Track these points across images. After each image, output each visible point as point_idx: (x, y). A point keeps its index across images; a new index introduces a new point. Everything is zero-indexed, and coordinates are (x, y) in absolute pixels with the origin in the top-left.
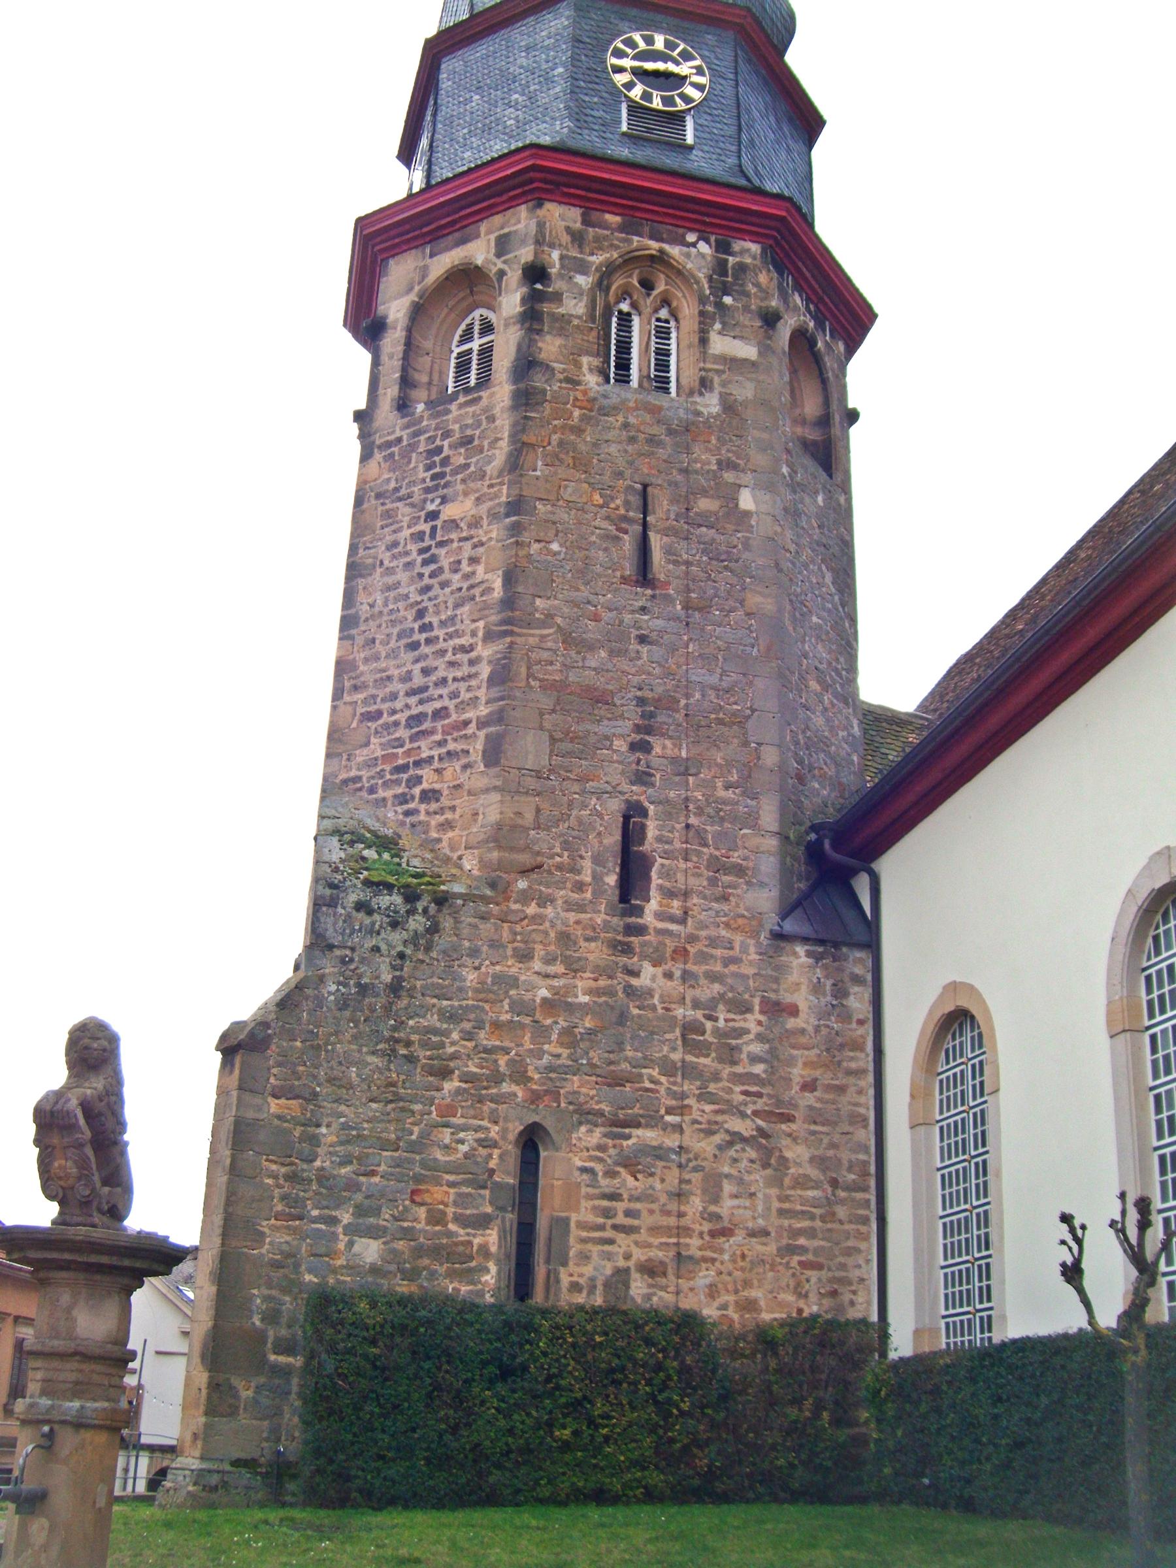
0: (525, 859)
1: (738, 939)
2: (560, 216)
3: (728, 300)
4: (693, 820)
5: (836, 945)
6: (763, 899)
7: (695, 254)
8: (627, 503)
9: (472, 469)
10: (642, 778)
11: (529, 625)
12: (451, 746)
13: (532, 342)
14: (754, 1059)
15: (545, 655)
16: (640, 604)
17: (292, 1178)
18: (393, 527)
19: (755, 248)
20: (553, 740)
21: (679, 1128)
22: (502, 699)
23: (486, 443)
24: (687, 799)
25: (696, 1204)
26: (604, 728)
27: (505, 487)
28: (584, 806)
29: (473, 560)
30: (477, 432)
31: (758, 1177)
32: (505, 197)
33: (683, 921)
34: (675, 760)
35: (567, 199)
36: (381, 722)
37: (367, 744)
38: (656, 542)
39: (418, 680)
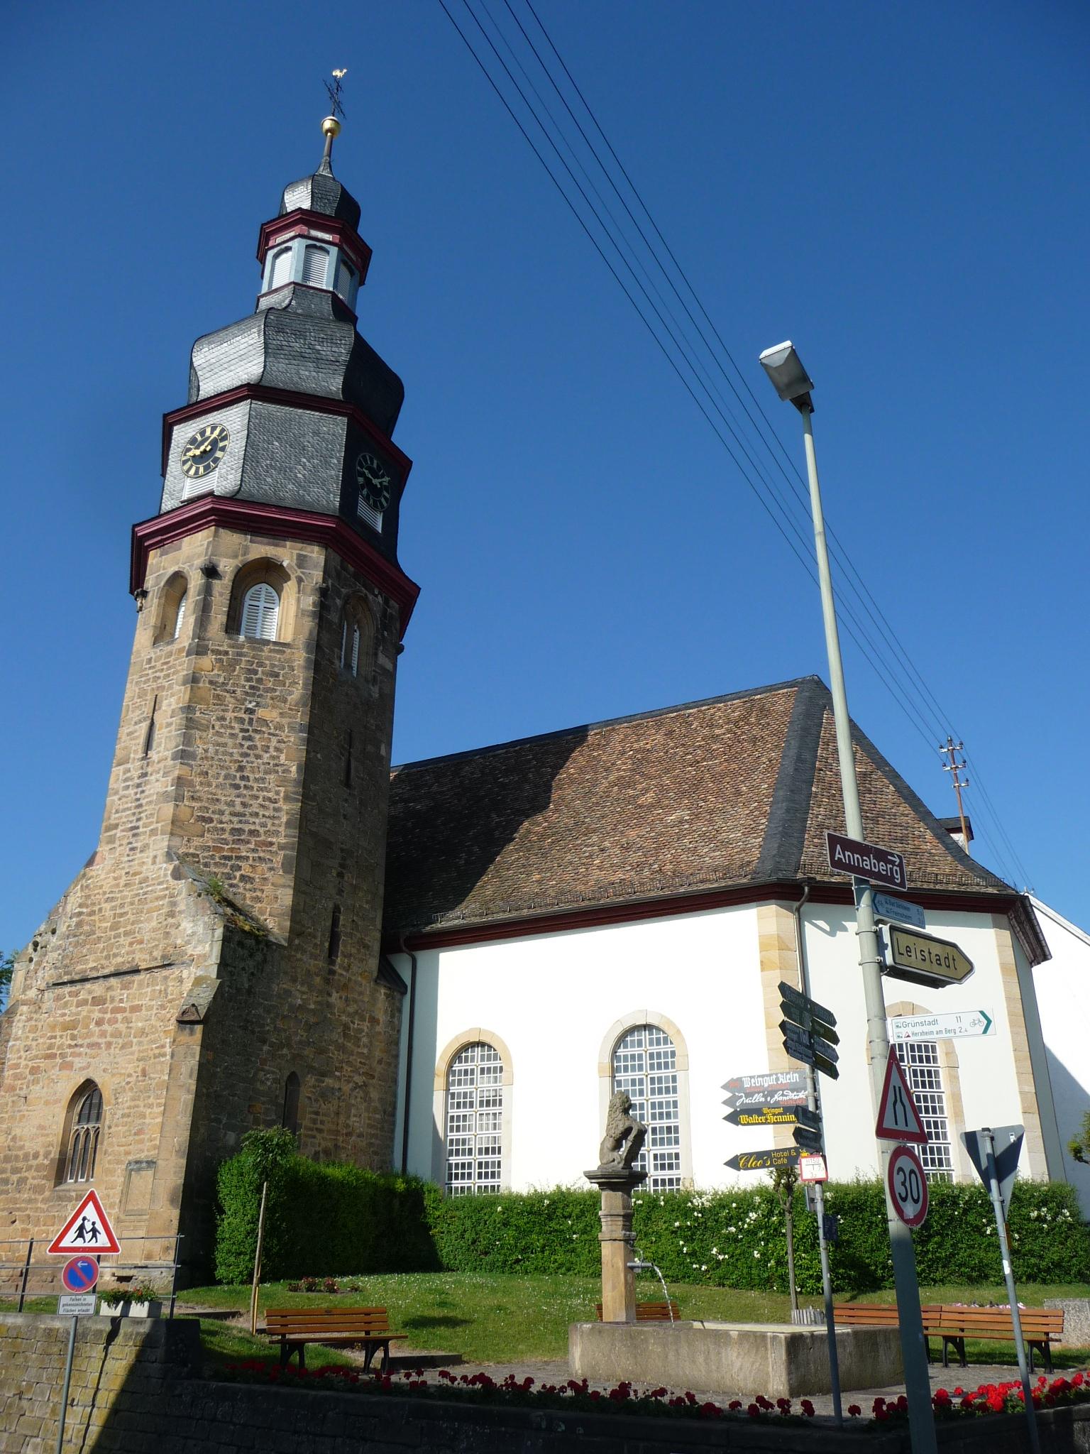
12: (262, 855)
21: (339, 1078)
23: (287, 682)
25: (342, 1119)
33: (347, 971)
37: (202, 836)
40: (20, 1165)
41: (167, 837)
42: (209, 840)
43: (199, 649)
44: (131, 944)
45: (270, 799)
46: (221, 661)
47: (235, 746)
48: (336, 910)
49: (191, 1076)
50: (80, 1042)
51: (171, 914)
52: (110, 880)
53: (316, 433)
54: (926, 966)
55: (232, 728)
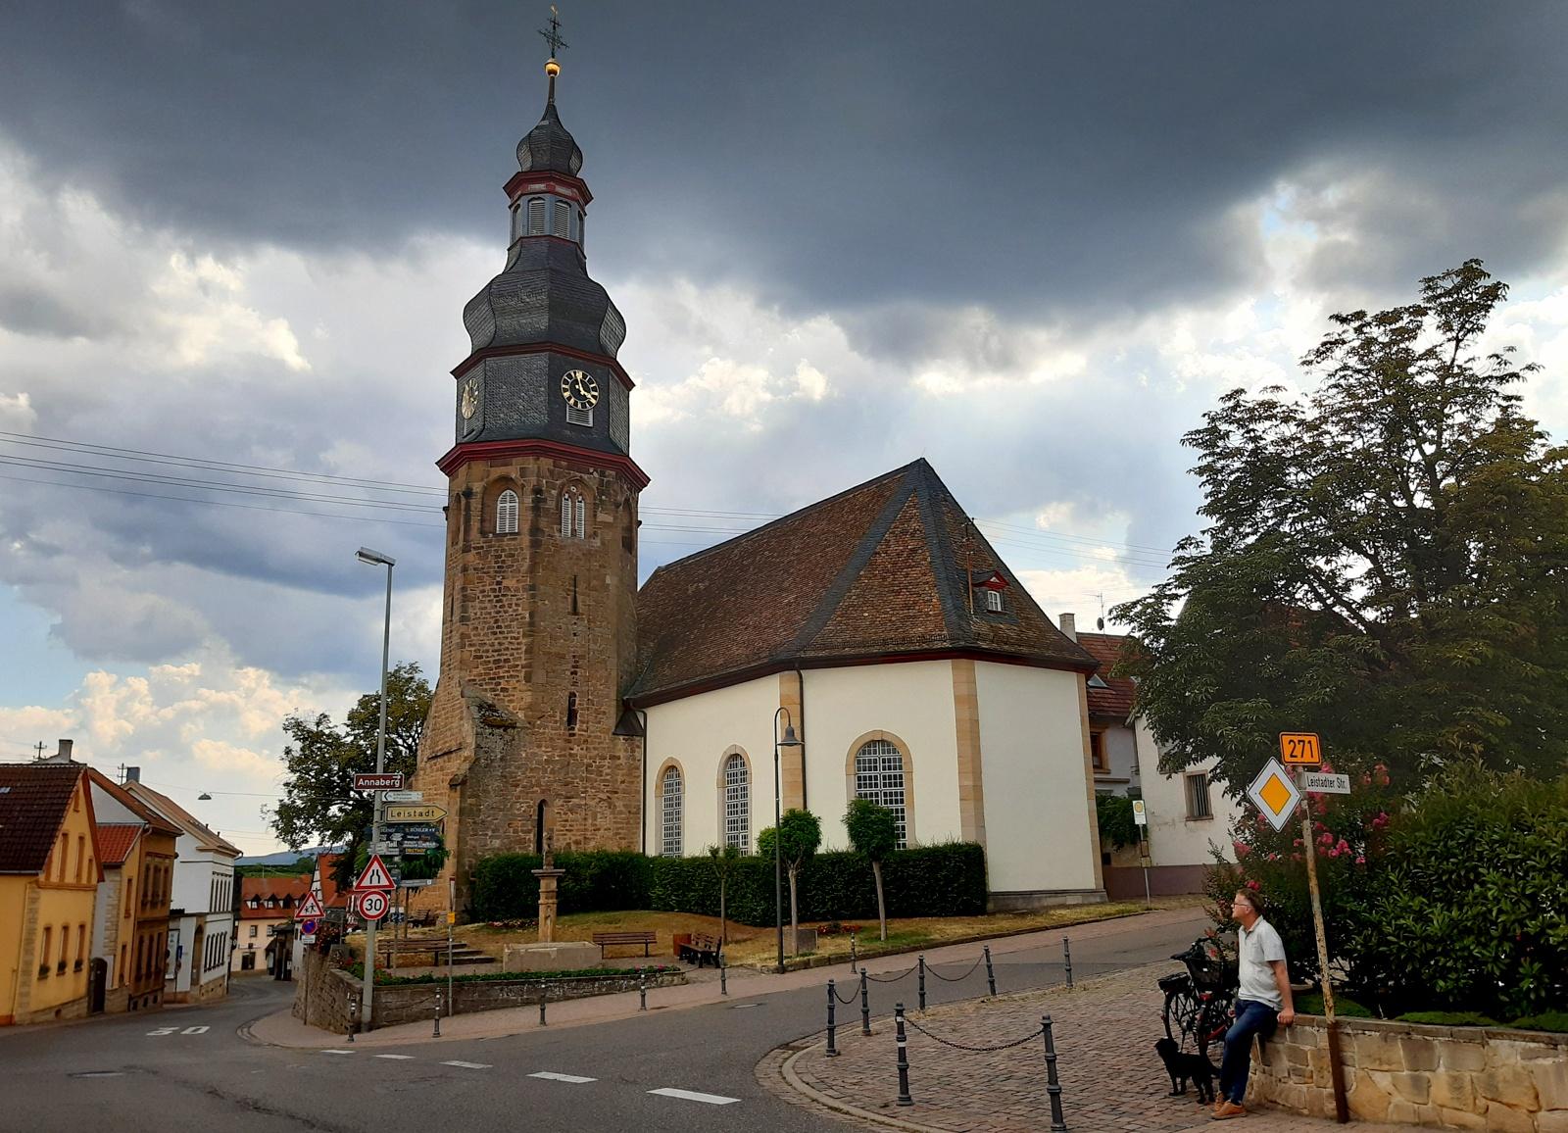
2: (546, 463)
3: (603, 497)
6: (610, 722)
12: (512, 673)
13: (537, 520)
17: (474, 823)
31: (608, 812)
35: (549, 457)
38: (580, 598)
39: (497, 647)
43: (466, 550)
48: (573, 695)
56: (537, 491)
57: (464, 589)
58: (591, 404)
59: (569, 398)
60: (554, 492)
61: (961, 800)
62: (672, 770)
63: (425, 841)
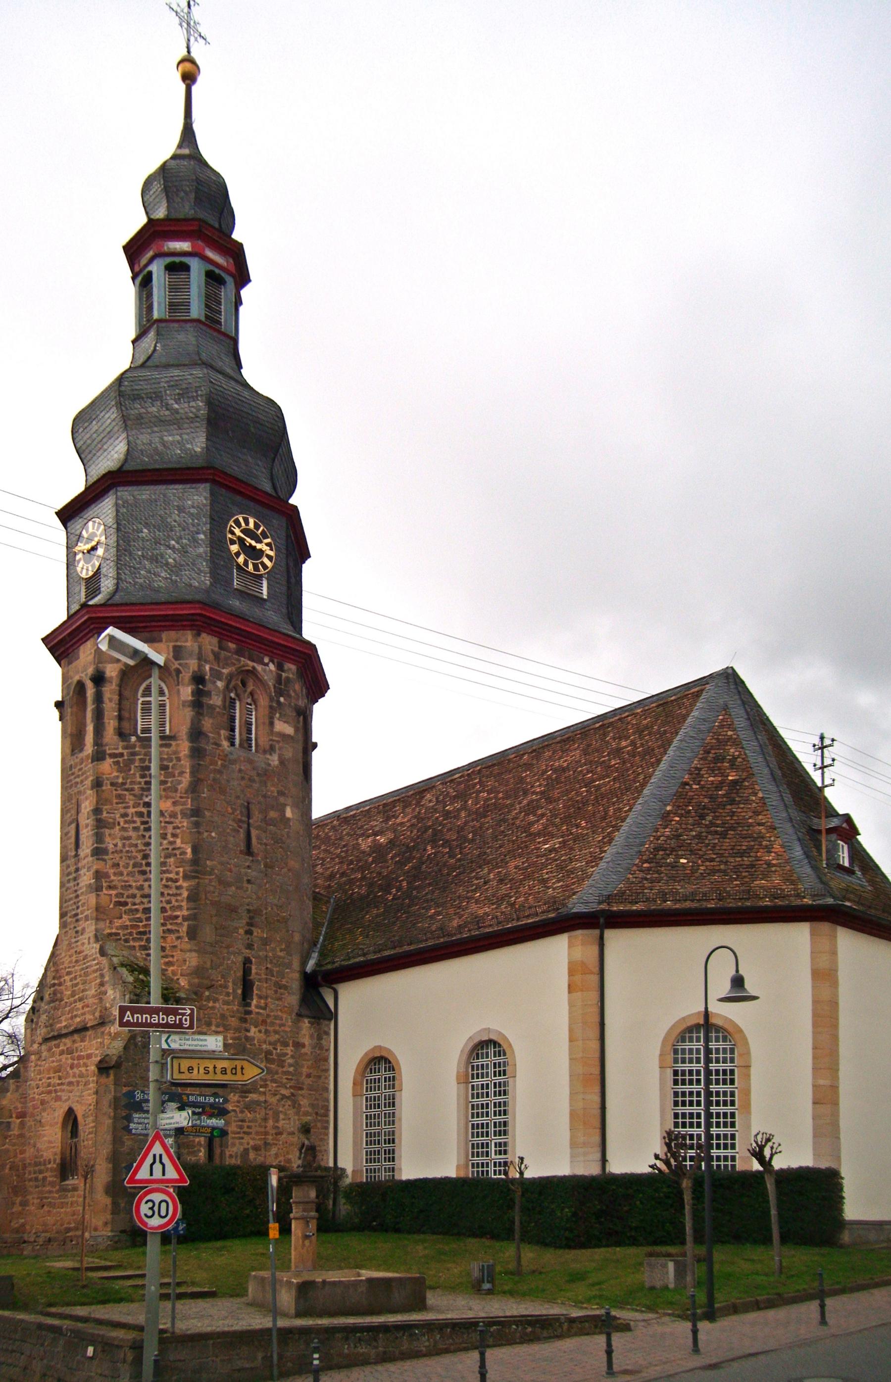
0: (206, 982)
1: (285, 1016)
2: (209, 642)
3: (282, 699)
4: (269, 966)
5: (319, 1019)
6: (293, 999)
7: (268, 669)
8: (241, 812)
9: (169, 785)
10: (250, 946)
11: (204, 874)
12: (169, 927)
13: (200, 720)
14: (290, 1065)
15: (212, 889)
16: (247, 864)
18: (124, 805)
19: (293, 667)
20: (216, 929)
21: (264, 1093)
22: (195, 909)
23: (177, 772)
24: (266, 956)
25: (270, 1123)
26: (235, 924)
27: (189, 800)
28: (229, 959)
29: (174, 835)
30: (171, 764)
31: (291, 1112)
32: (179, 623)
33: (265, 1009)
34: (262, 939)
35: (212, 633)
36: (127, 907)
37: (121, 918)
38: (254, 833)
40: (42, 1167)
41: (94, 922)
42: (126, 920)
43: (99, 756)
44: (83, 1008)
45: (171, 880)
46: (117, 763)
47: (138, 838)
48: (247, 962)
49: (110, 1106)
50: (63, 1081)
51: (102, 984)
52: (67, 957)
53: (181, 509)
54: (211, 1076)
55: (134, 822)
56: (198, 679)
57: (97, 811)
58: (265, 567)
59: (238, 554)
60: (220, 684)
61: (814, 1103)
62: (379, 1064)
63: (211, 1116)
